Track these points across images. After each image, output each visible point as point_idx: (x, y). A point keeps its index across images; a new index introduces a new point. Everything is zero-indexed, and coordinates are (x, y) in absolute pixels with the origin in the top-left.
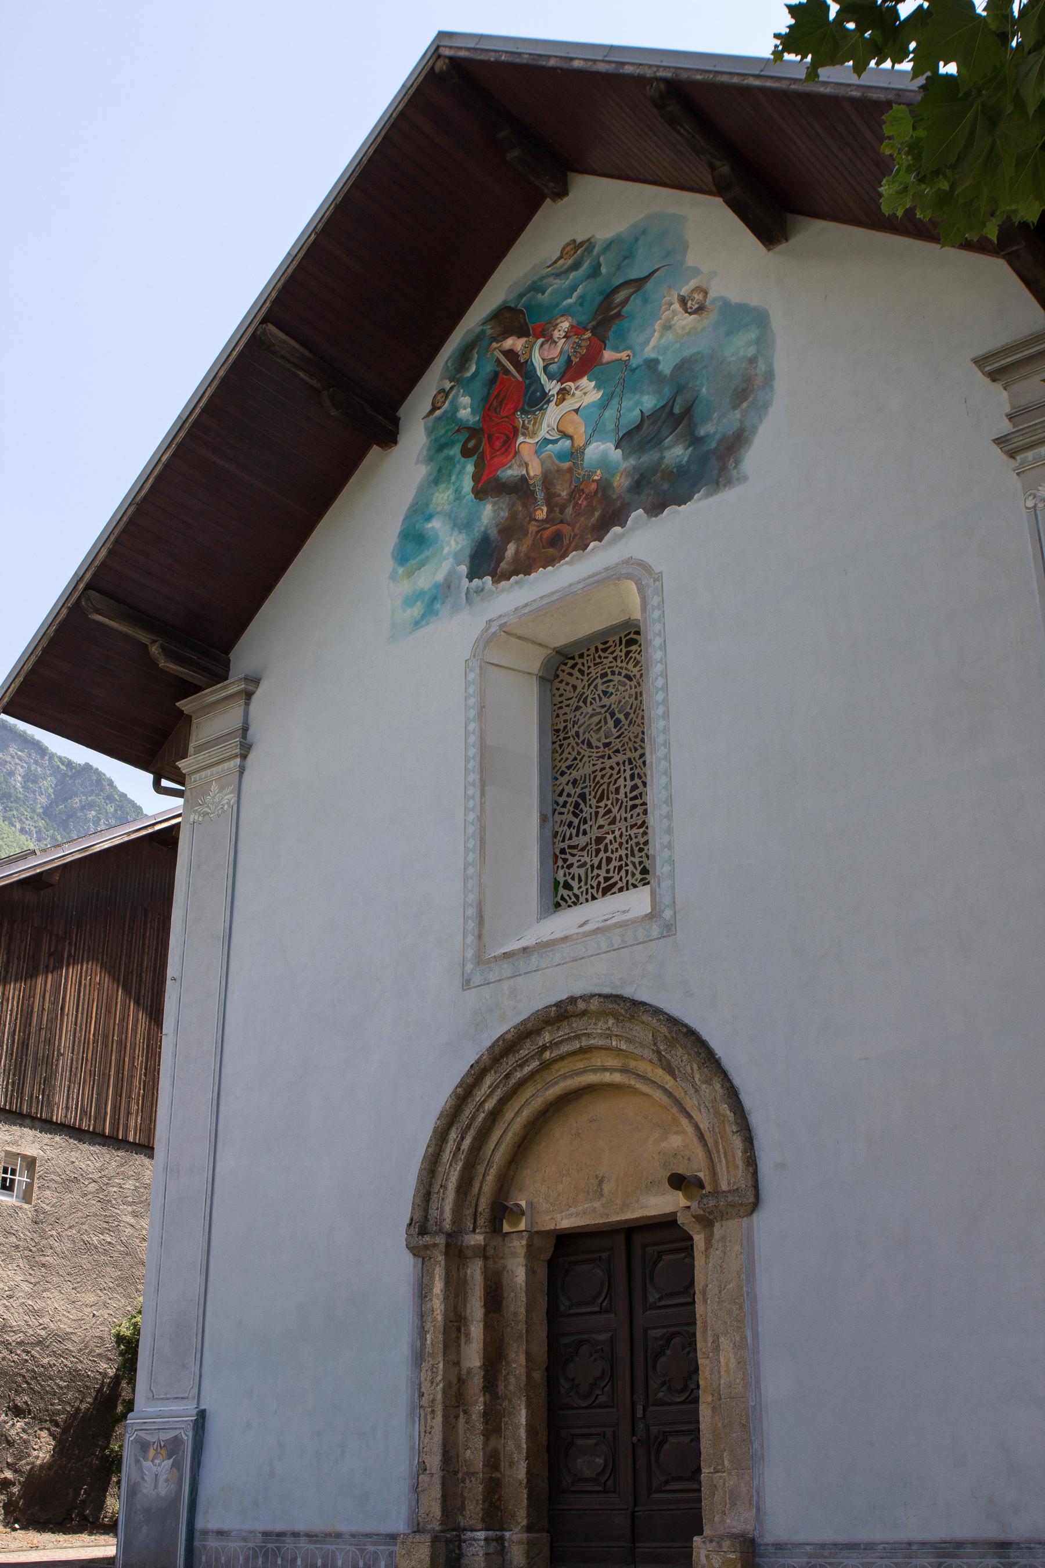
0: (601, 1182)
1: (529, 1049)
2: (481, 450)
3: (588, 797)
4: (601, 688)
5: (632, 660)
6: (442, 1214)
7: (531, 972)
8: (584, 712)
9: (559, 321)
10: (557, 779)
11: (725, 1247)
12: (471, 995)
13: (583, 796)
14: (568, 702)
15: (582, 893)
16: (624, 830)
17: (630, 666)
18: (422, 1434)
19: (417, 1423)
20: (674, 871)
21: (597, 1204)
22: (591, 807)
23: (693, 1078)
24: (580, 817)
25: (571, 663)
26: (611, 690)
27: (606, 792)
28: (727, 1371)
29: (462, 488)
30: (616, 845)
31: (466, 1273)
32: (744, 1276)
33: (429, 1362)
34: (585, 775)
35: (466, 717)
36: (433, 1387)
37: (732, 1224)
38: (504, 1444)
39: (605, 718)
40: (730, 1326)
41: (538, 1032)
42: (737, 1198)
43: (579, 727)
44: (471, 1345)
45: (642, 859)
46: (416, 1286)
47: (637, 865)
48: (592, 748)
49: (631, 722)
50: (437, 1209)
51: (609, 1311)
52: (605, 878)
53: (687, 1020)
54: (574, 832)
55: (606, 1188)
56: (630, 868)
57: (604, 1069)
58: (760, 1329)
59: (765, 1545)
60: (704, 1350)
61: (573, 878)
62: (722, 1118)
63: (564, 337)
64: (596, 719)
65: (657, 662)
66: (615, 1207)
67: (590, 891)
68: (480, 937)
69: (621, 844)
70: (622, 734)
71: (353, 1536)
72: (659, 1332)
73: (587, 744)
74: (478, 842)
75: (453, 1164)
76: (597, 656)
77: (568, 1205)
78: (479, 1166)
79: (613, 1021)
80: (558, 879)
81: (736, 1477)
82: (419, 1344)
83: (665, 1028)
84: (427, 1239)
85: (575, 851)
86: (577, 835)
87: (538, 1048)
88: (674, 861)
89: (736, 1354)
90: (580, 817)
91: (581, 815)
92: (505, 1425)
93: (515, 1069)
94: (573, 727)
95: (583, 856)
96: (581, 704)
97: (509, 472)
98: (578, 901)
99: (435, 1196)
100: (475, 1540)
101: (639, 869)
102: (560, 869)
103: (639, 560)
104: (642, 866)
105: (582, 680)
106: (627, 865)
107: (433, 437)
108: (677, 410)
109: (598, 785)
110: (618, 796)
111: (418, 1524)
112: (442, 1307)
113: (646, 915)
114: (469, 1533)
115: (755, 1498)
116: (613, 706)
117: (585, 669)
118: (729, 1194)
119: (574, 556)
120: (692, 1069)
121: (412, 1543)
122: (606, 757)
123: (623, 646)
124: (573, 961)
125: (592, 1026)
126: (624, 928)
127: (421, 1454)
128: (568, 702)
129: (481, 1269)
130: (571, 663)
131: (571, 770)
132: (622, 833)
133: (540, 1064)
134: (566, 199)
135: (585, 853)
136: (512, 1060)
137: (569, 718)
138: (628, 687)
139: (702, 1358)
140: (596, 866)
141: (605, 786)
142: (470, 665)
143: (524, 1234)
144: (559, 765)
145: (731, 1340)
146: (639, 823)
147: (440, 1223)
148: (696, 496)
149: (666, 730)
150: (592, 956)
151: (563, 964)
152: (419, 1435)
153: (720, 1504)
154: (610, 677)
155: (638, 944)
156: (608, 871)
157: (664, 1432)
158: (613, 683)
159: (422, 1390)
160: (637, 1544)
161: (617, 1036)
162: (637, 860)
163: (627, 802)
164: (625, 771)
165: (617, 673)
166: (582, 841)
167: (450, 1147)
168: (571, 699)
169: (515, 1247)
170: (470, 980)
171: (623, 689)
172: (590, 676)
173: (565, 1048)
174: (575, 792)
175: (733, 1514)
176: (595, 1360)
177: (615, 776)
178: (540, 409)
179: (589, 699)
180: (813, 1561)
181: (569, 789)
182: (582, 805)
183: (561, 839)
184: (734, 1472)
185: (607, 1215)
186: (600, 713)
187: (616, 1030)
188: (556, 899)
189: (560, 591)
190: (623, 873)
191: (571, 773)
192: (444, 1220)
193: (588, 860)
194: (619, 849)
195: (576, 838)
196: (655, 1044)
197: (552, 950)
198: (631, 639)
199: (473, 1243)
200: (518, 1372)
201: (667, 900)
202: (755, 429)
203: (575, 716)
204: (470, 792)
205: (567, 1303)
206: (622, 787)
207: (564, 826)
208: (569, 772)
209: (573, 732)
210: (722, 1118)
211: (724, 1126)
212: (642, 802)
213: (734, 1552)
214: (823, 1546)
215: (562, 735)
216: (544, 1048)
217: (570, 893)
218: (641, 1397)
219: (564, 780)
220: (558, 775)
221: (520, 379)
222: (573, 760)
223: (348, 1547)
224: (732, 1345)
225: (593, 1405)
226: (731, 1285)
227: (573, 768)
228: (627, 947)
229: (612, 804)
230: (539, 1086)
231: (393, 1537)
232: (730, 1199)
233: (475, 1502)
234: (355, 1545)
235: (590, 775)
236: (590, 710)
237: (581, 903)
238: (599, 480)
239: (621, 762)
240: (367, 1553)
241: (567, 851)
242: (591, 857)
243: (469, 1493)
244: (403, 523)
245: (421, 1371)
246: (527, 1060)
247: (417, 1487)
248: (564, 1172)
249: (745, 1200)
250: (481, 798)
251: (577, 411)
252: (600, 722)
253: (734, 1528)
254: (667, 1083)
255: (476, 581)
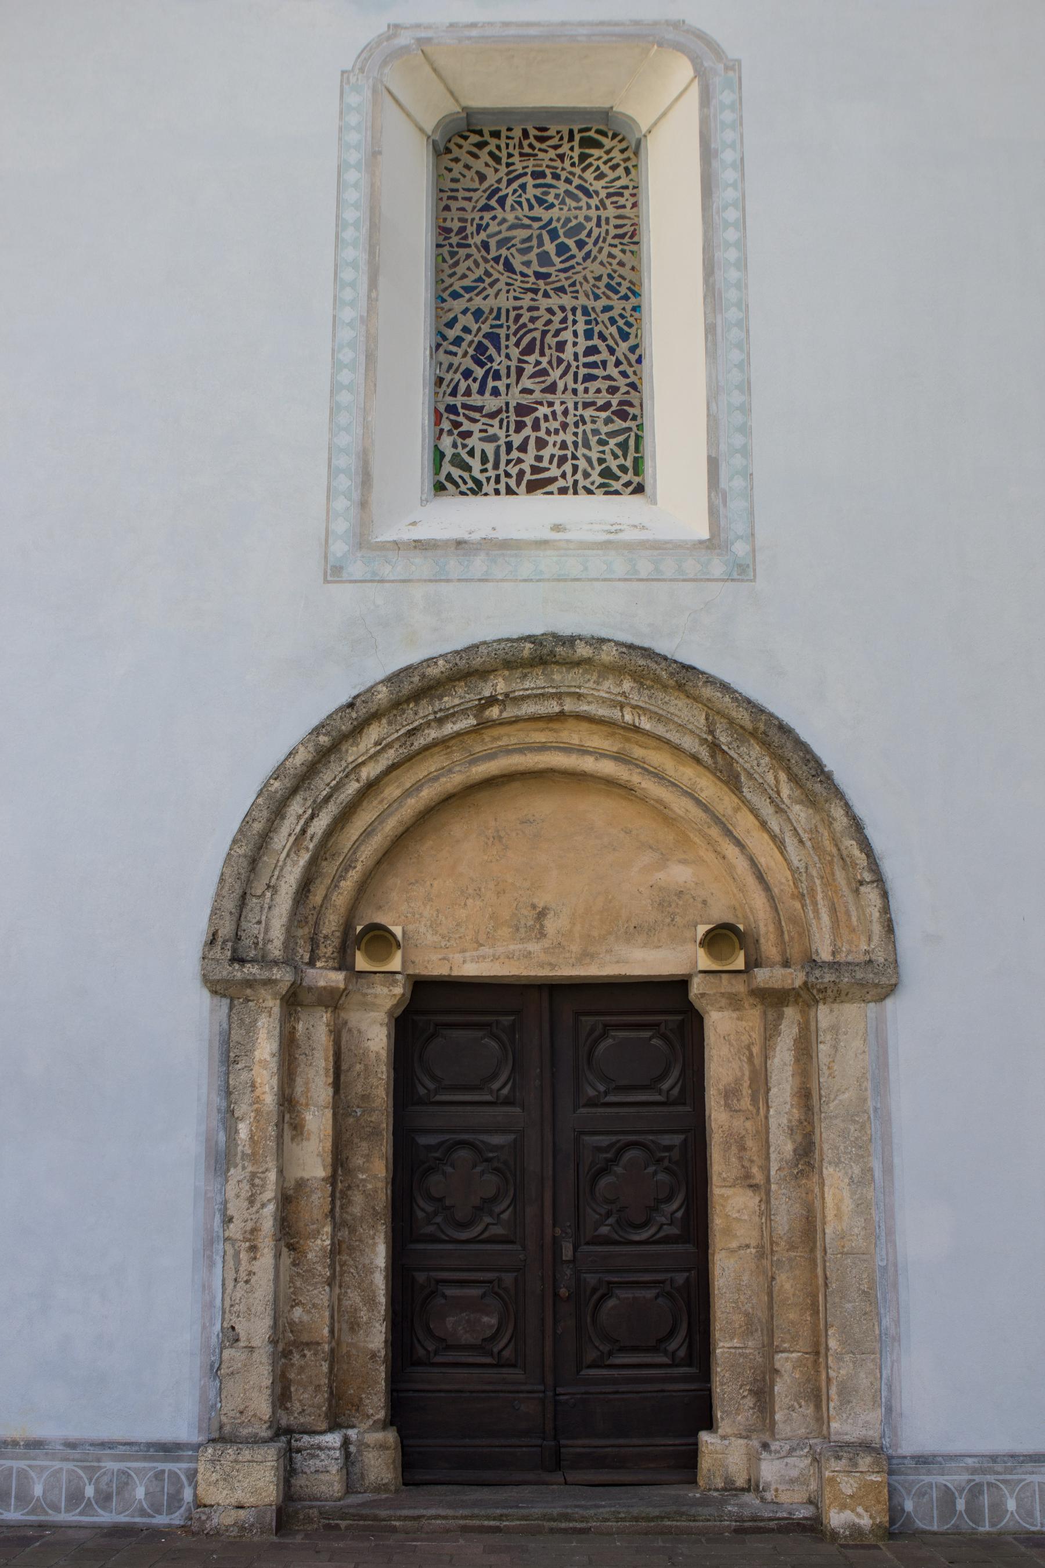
0: (542, 915)
1: (461, 697)
4: (531, 192)
6: (267, 930)
7: (471, 580)
8: (500, 217)
11: (836, 1040)
12: (343, 594)
14: (467, 194)
15: (488, 479)
16: (571, 406)
17: (589, 175)
18: (230, 1284)
19: (220, 1265)
20: (752, 489)
21: (534, 947)
23: (778, 793)
24: (487, 367)
25: (475, 138)
26: (550, 198)
27: (538, 343)
28: (838, 1216)
31: (294, 1028)
32: (869, 1085)
33: (244, 1168)
34: (499, 309)
36: (254, 1209)
37: (850, 1011)
38: (339, 1295)
39: (540, 237)
40: (845, 1153)
41: (483, 674)
42: (871, 975)
44: (305, 1143)
46: (216, 1044)
47: (595, 463)
49: (588, 255)
50: (259, 922)
51: (508, 1102)
52: (532, 466)
53: (771, 708)
54: (475, 387)
55: (551, 925)
56: (582, 464)
57: (583, 751)
58: (896, 1161)
59: (899, 1457)
60: (724, 1175)
62: (828, 858)
64: (524, 234)
66: (568, 955)
67: (503, 479)
68: (364, 504)
69: (565, 426)
70: (573, 267)
71: (71, 1445)
72: (604, 1140)
73: (504, 264)
75: (292, 855)
76: (525, 143)
77: (477, 942)
78: (324, 863)
79: (632, 684)
81: (851, 1365)
82: (222, 1137)
83: (745, 714)
84: (254, 971)
85: (476, 415)
86: (481, 392)
87: (480, 699)
88: (751, 474)
89: (853, 1193)
90: (487, 367)
92: (341, 1266)
93: (428, 724)
95: (492, 426)
96: (493, 202)
98: (480, 489)
99: (254, 900)
100: (320, 1448)
101: (598, 469)
102: (445, 435)
104: (604, 466)
105: (496, 170)
106: (574, 457)
109: (524, 330)
111: (221, 1428)
112: (275, 1081)
114: (306, 1438)
115: (884, 1393)
116: (554, 224)
117: (503, 155)
118: (857, 968)
120: (776, 778)
121: (236, 1461)
122: (541, 293)
125: (591, 684)
126: (658, 552)
127: (227, 1316)
128: (467, 194)
129: (328, 1025)
130: (475, 138)
131: (472, 294)
133: (478, 725)
135: (496, 422)
136: (426, 709)
138: (583, 204)
139: (721, 1187)
140: (516, 445)
141: (537, 335)
142: (353, 80)
143: (399, 977)
145: (846, 1173)
146: (600, 403)
147: (264, 944)
149: (741, 285)
150: (597, 580)
151: (539, 581)
152: (223, 1285)
153: (786, 1396)
154: (549, 180)
155: (684, 580)
157: (609, 1283)
158: (557, 191)
159: (229, 1213)
160: (563, 1442)
161: (634, 707)
162: (594, 456)
163: (577, 367)
164: (575, 322)
165: (563, 178)
166: (492, 404)
167: (289, 825)
168: (475, 190)
169: (376, 996)
170: (341, 568)
171: (574, 204)
172: (511, 168)
173: (529, 709)
174: (479, 329)
175: (844, 1415)
176: (483, 1173)
179: (509, 202)
180: (977, 1478)
181: (468, 320)
182: (492, 351)
183: (449, 391)
184: (847, 1358)
185: (553, 966)
186: (529, 227)
187: (635, 698)
188: (437, 478)
190: (568, 467)
191: (470, 300)
192: (271, 941)
195: (479, 397)
196: (711, 732)
198: (590, 138)
199: (322, 983)
200: (369, 1186)
201: (740, 527)
204: (348, 275)
205: (431, 1086)
210: (828, 858)
211: (832, 869)
212: (605, 374)
213: (878, 1472)
214: (994, 1458)
215: (455, 240)
216: (492, 701)
217: (466, 475)
218: (569, 1231)
219: (458, 305)
220: (445, 295)
222: (475, 281)
223: (57, 1465)
224: (847, 1180)
225: (481, 1238)
226: (846, 1095)
227: (476, 292)
229: (550, 363)
230: (457, 756)
231: (168, 1450)
232: (859, 975)
233: (311, 1389)
234: (74, 1460)
236: (511, 217)
237: (486, 494)
239: (569, 308)
240: (105, 1473)
242: (507, 431)
243: (299, 1374)
245: (227, 1181)
246: (453, 715)
247: (219, 1369)
248: (470, 891)
249: (884, 979)
250: (370, 291)
252: (529, 239)
253: (846, 1434)
254: (702, 790)
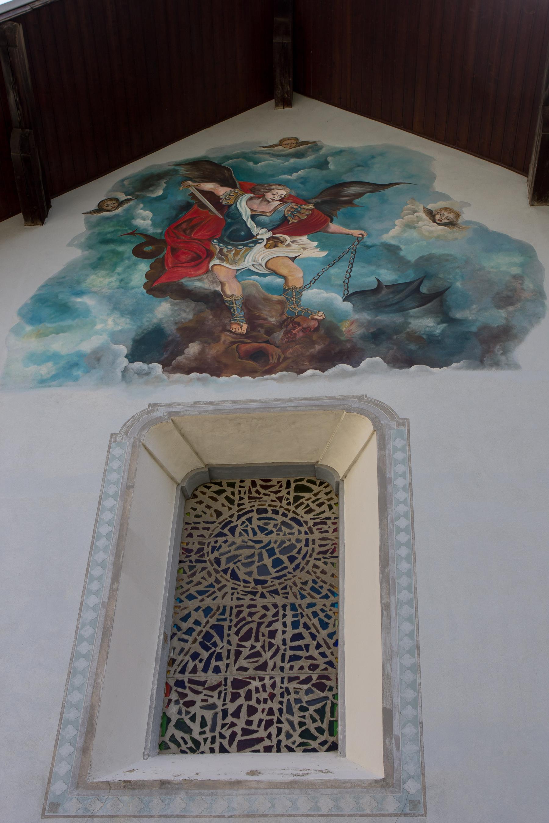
2: (161, 256)
3: (226, 632)
4: (255, 523)
5: (304, 506)
9: (273, 187)
10: (183, 601)
13: (219, 629)
15: (205, 740)
16: (278, 680)
20: (422, 735)
22: (229, 642)
24: (212, 651)
25: (216, 488)
26: (270, 527)
27: (254, 632)
29: (131, 280)
30: (265, 695)
34: (225, 607)
35: (102, 490)
39: (260, 554)
43: (221, 555)
45: (303, 720)
47: (297, 726)
48: (238, 580)
52: (243, 729)
54: (201, 666)
61: (193, 719)
63: (279, 200)
65: (400, 502)
67: (218, 740)
68: (85, 750)
73: (231, 575)
74: (100, 633)
80: (168, 714)
85: (200, 688)
86: (205, 670)
88: (421, 723)
90: (212, 651)
91: (214, 649)
94: (212, 552)
95: (212, 697)
97: (198, 284)
101: (299, 731)
102: (172, 704)
103: (377, 401)
105: (230, 509)
106: (279, 721)
107: (96, 230)
108: (424, 289)
109: (244, 622)
110: (272, 641)
113: (377, 781)
119: (284, 375)
123: (292, 489)
124: (248, 816)
128: (207, 526)
130: (216, 488)
131: (204, 596)
132: (275, 682)
134: (287, 109)
135: (215, 694)
137: (207, 542)
138: (295, 530)
140: (230, 712)
141: (254, 626)
144: (186, 587)
146: (302, 677)
148: (454, 365)
150: (282, 816)
156: (249, 723)
158: (275, 522)
162: (296, 720)
166: (212, 679)
170: (59, 804)
174: (208, 622)
177: (269, 618)
178: (244, 245)
179: (238, 530)
181: (200, 616)
182: (216, 638)
186: (253, 547)
188: (163, 739)
189: (262, 402)
190: (273, 730)
191: (202, 600)
193: (219, 703)
194: (269, 701)
195: (203, 674)
197: (212, 794)
201: (411, 768)
202: (525, 331)
203: (216, 542)
204: (96, 572)
206: (279, 633)
207: (185, 655)
208: (200, 598)
209: (212, 557)
215: (194, 557)
217: (187, 737)
219: (192, 605)
220: (183, 597)
221: (221, 216)
227: (207, 594)
228: (343, 816)
229: (263, 647)
235: (231, 608)
237: (203, 752)
238: (321, 320)
239: (280, 605)
241: (187, 685)
242: (224, 700)
244: (40, 289)
250: (112, 583)
251: (293, 259)
252: (252, 556)
255: (138, 365)
